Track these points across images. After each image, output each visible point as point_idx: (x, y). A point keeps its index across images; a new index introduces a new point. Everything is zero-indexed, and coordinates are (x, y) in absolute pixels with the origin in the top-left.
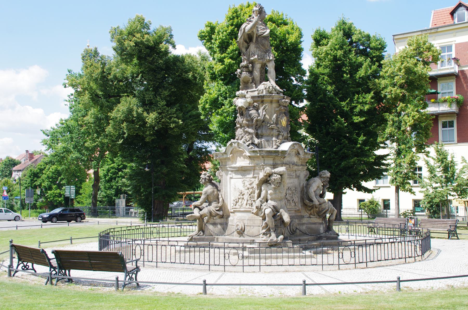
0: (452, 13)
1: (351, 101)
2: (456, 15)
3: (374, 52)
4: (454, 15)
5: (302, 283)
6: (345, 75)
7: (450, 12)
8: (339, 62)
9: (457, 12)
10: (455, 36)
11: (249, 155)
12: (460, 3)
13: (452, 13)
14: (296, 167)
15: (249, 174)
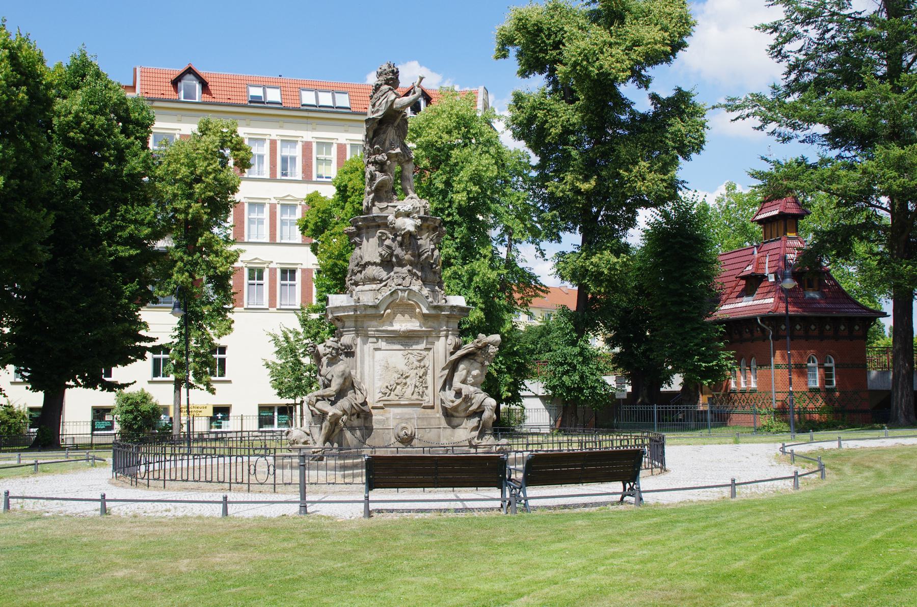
0: (175, 83)
1: (113, 216)
2: (181, 85)
3: (137, 131)
4: (179, 84)
5: (730, 482)
6: (107, 165)
7: (173, 77)
8: (97, 138)
9: (183, 82)
10: (179, 121)
11: (427, 312)
12: (190, 68)
13: (175, 83)
15: (417, 343)
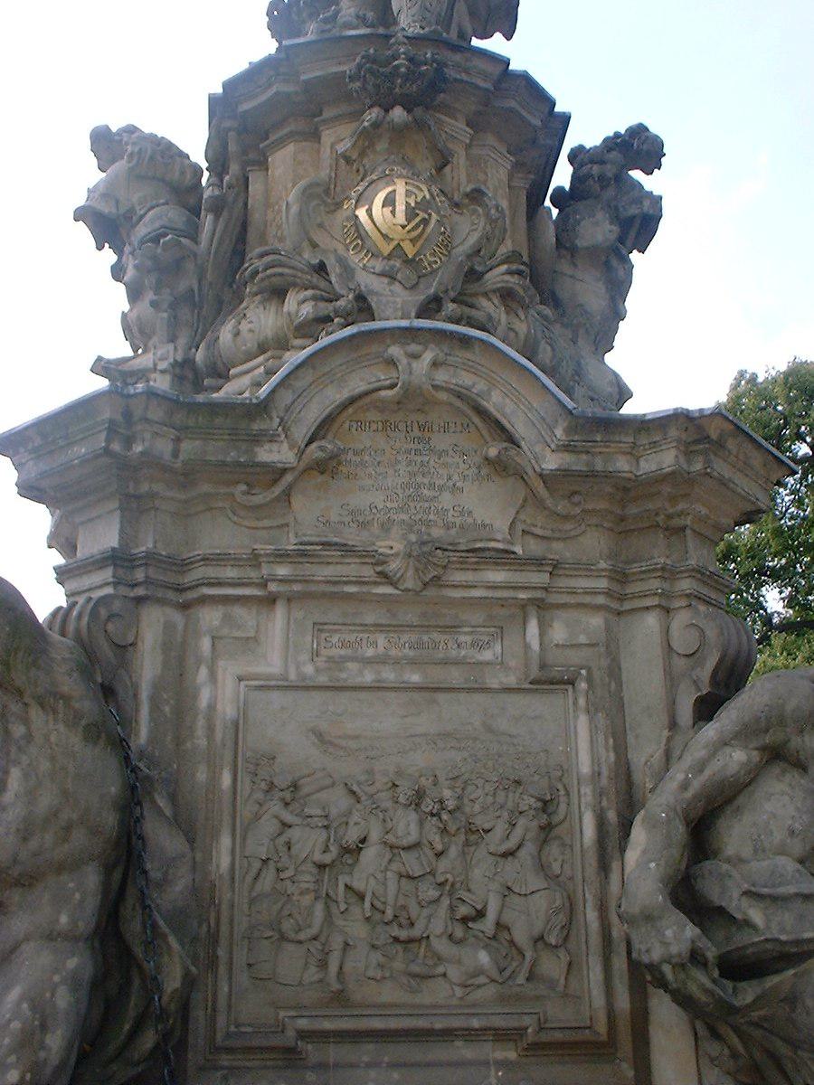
14: (497, 576)
